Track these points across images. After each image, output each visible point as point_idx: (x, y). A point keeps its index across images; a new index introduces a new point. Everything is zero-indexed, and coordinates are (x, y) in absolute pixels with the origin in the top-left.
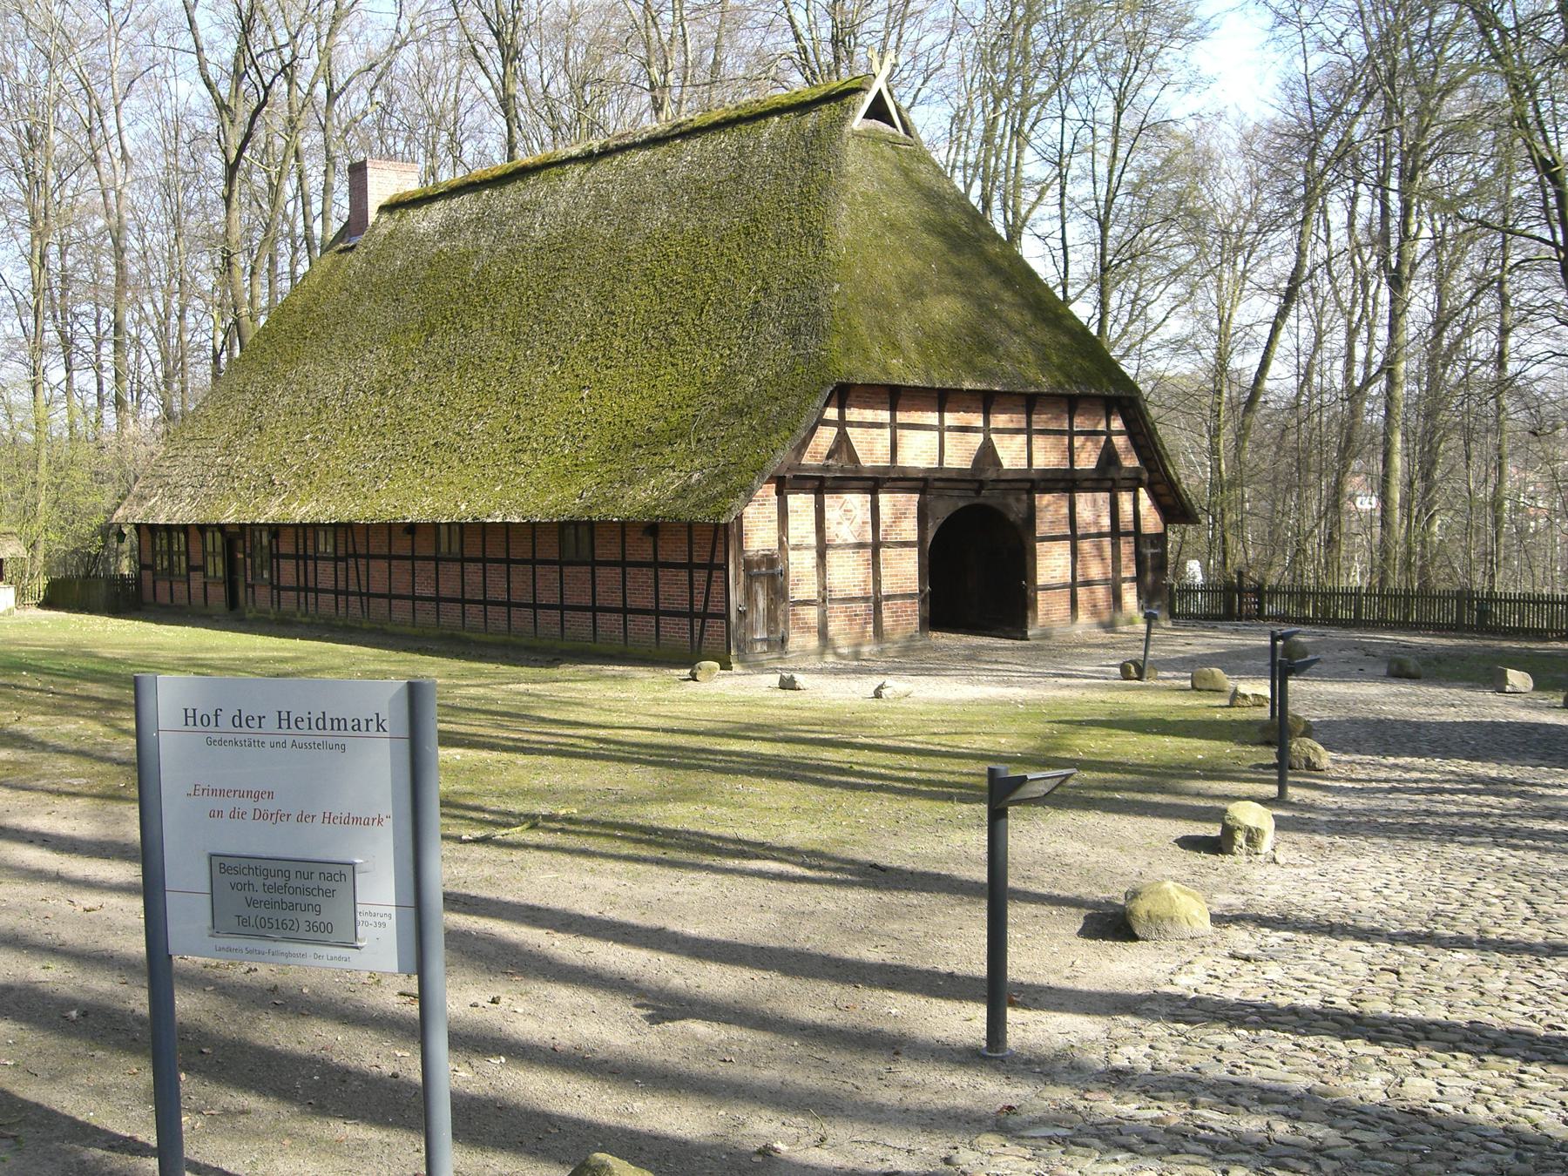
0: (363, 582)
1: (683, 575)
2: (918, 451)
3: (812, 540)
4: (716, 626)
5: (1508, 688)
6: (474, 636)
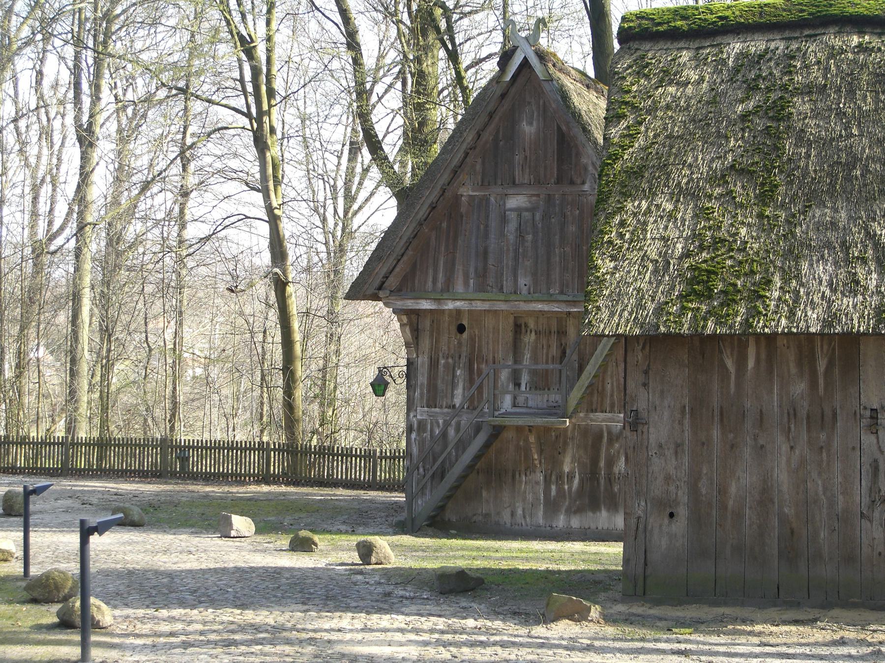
5: (233, 533)
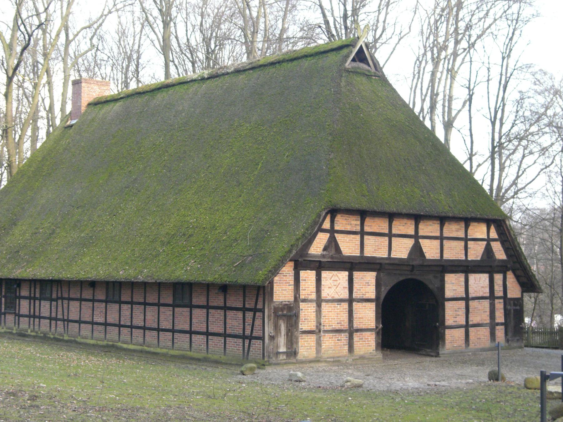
0: (66, 314)
1: (240, 314)
2: (376, 248)
3: (313, 296)
4: (257, 344)
6: (125, 346)
